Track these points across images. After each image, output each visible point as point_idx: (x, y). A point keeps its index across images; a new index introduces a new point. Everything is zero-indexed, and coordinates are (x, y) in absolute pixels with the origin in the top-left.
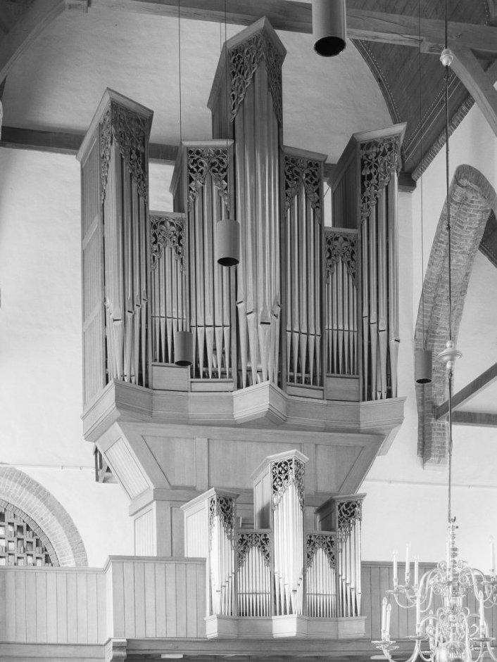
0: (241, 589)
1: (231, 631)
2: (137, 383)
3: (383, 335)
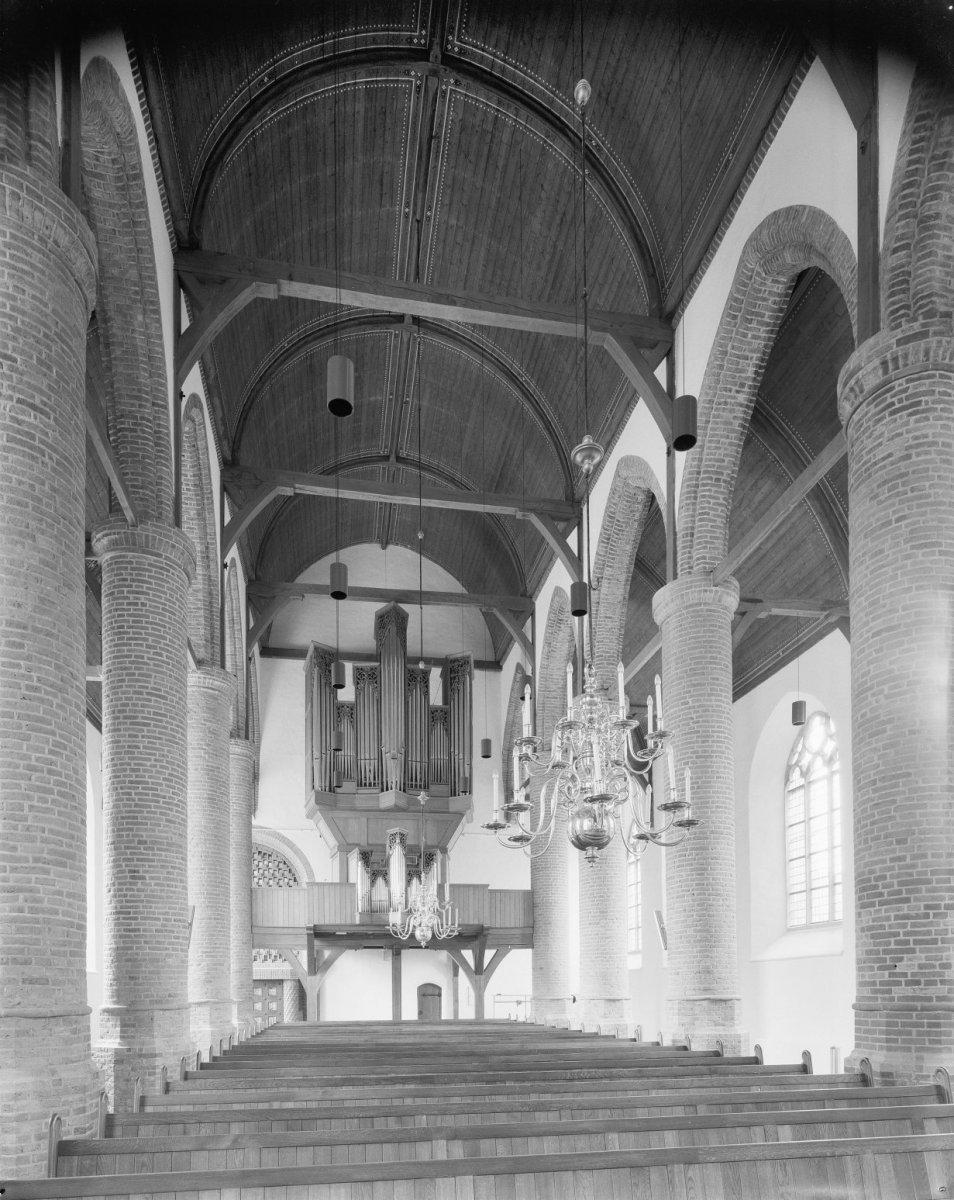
0: (373, 899)
1: (367, 920)
2: (327, 789)
3: (461, 761)
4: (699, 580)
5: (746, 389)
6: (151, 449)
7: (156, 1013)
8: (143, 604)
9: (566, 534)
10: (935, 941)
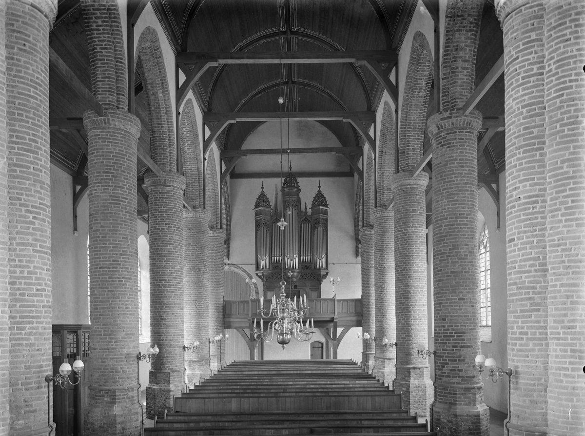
8: (164, 207)
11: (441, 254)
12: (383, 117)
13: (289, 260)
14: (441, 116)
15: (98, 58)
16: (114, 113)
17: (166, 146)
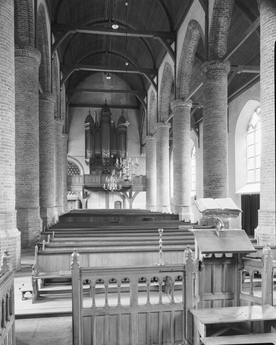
4: (181, 101)
5: (191, 54)
6: (46, 75)
7: (47, 208)
9: (144, 98)
10: (216, 194)
11: (209, 137)
12: (164, 71)
13: (105, 153)
14: (210, 63)
15: (19, 14)
16: (28, 48)
17: (46, 77)
